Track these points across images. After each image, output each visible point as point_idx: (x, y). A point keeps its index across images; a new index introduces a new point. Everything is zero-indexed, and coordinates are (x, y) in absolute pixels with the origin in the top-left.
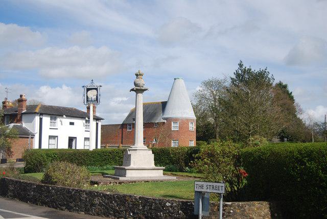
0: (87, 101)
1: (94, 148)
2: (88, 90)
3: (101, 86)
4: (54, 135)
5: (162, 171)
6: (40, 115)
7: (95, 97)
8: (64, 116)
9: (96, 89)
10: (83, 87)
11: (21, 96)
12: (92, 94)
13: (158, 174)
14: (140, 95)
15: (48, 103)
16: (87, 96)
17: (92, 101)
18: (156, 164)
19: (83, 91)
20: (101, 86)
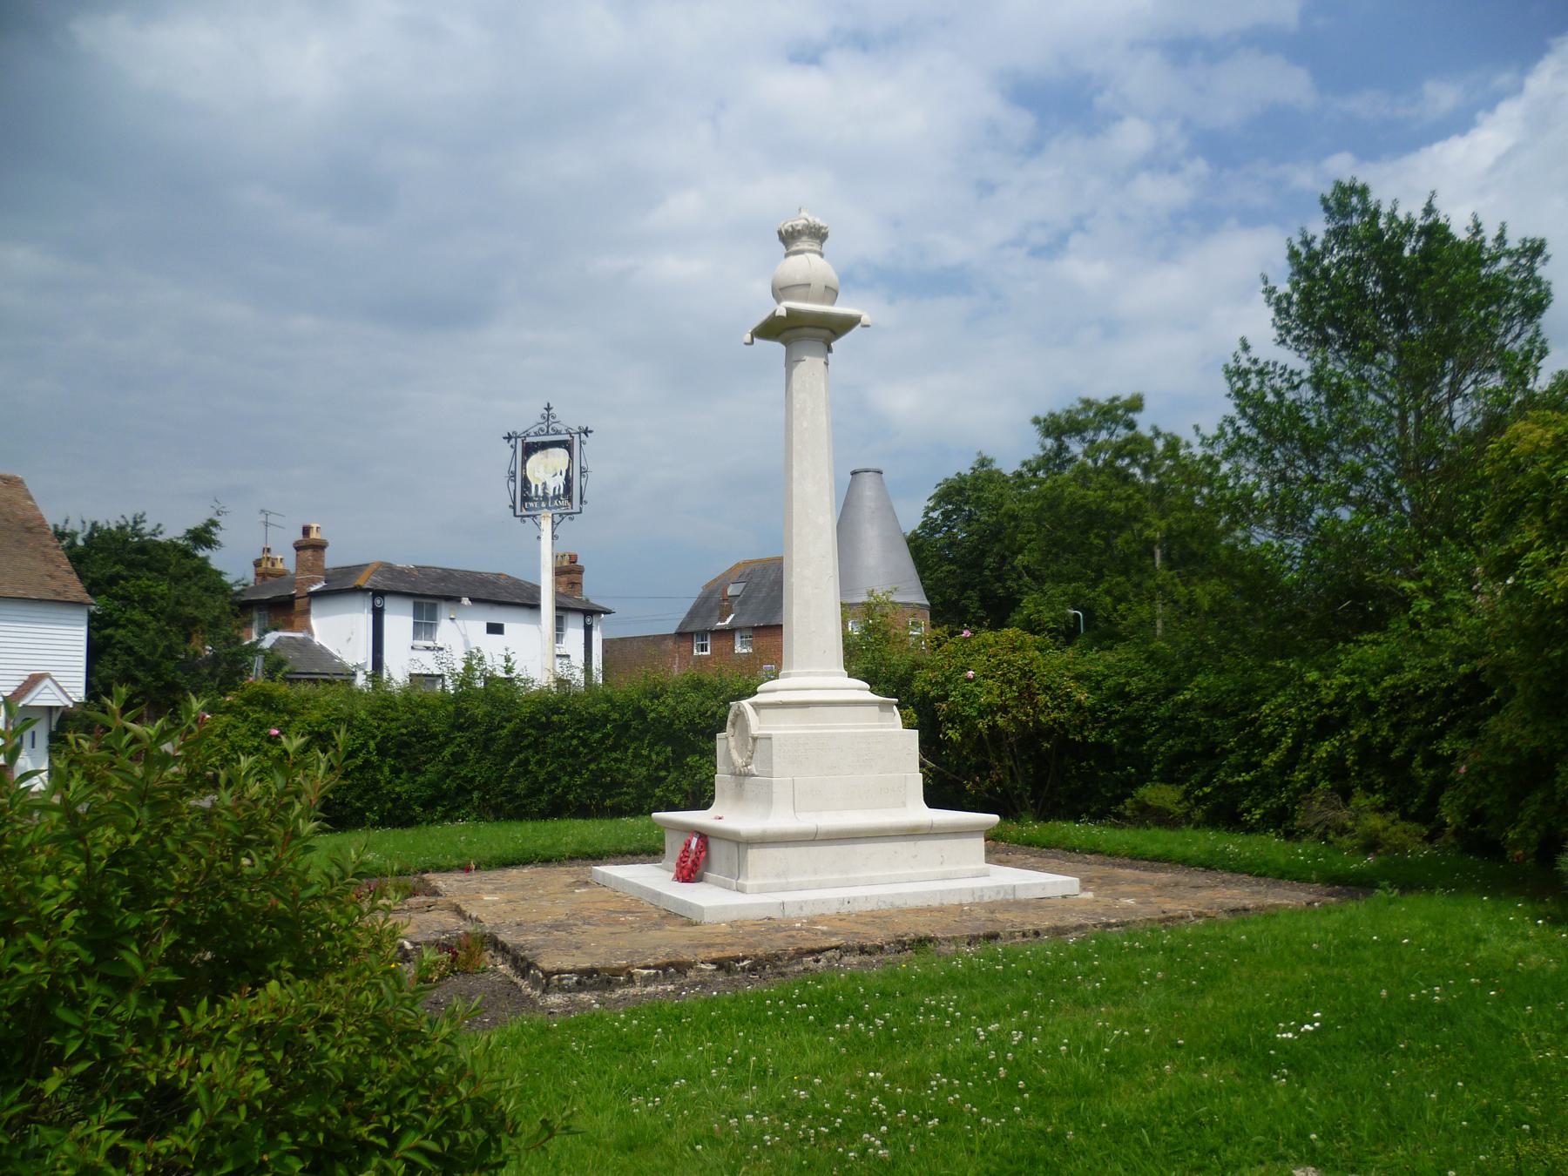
0: (525, 499)
1: (389, 620)
2: (530, 449)
3: (586, 432)
4: (236, 588)
5: (979, 844)
6: (374, 597)
7: (561, 480)
8: (466, 601)
9: (566, 445)
10: (509, 438)
11: (306, 531)
12: (546, 470)
13: (956, 872)
14: (810, 367)
15: (404, 558)
16: (525, 481)
17: (545, 497)
18: (935, 797)
19: (505, 454)
20: (586, 432)
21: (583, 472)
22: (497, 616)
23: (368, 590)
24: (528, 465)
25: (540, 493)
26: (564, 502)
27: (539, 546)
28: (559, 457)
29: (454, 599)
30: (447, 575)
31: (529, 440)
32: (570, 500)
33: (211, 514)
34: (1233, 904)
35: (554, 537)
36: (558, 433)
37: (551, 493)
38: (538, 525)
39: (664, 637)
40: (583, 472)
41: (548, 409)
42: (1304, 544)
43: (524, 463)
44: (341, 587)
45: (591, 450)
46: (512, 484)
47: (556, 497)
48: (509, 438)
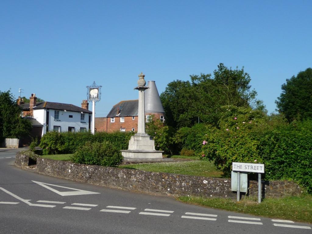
2: (91, 89)
3: (101, 87)
7: (96, 95)
9: (98, 89)
10: (87, 87)
16: (90, 94)
17: (94, 98)
19: (86, 90)
21: (100, 94)
22: (71, 114)
23: (46, 108)
24: (91, 92)
25: (93, 97)
26: (97, 99)
27: (92, 106)
28: (96, 91)
29: (63, 110)
30: (60, 105)
31: (91, 87)
32: (98, 98)
33: (9, 89)
34: (63, 159)
35: (95, 105)
36: (96, 86)
37: (94, 97)
38: (92, 103)
39: (104, 118)
40: (100, 94)
41: (94, 82)
42: (216, 127)
43: (90, 91)
44: (39, 104)
45: (102, 90)
46: (88, 95)
47: (96, 98)
48: (87, 87)
